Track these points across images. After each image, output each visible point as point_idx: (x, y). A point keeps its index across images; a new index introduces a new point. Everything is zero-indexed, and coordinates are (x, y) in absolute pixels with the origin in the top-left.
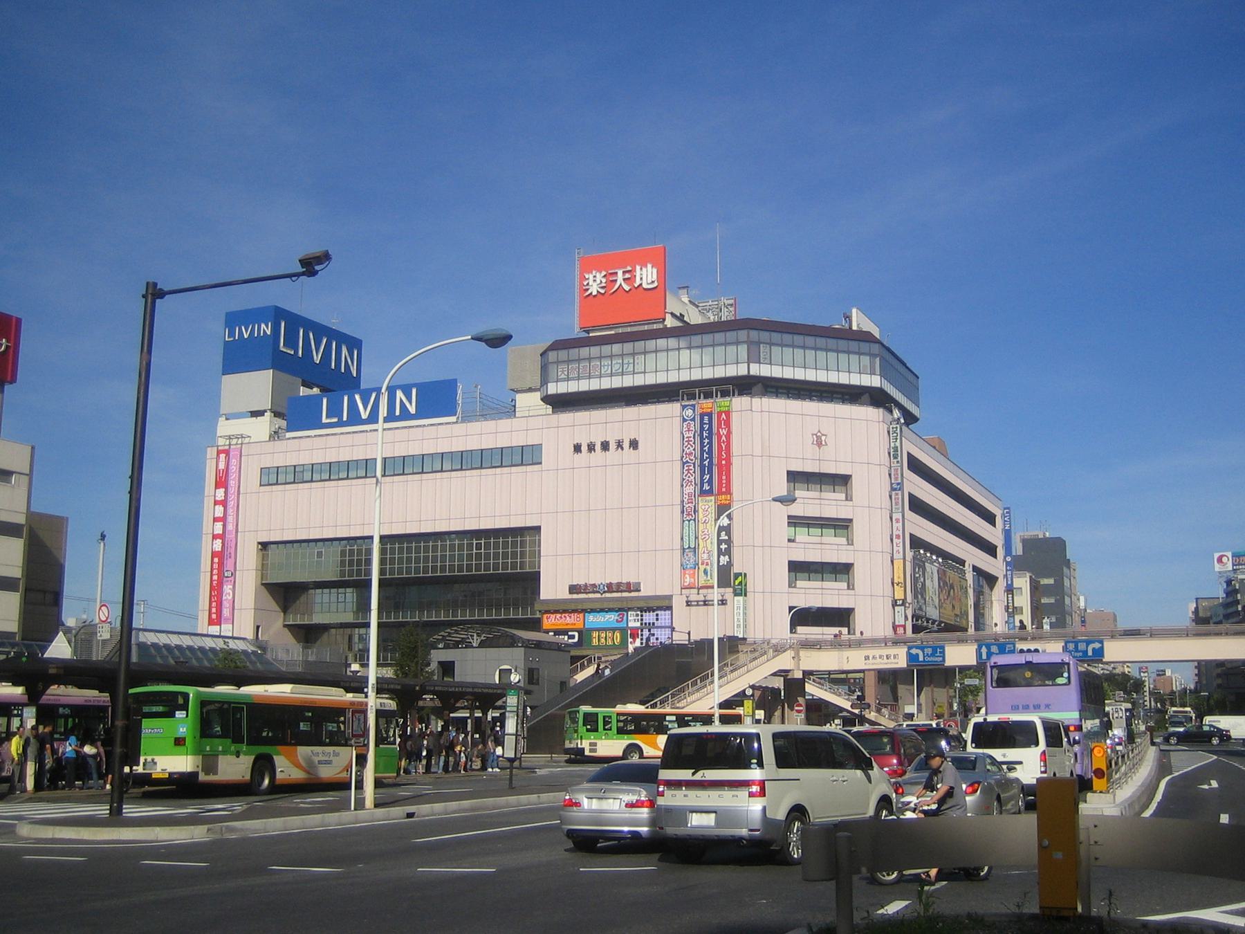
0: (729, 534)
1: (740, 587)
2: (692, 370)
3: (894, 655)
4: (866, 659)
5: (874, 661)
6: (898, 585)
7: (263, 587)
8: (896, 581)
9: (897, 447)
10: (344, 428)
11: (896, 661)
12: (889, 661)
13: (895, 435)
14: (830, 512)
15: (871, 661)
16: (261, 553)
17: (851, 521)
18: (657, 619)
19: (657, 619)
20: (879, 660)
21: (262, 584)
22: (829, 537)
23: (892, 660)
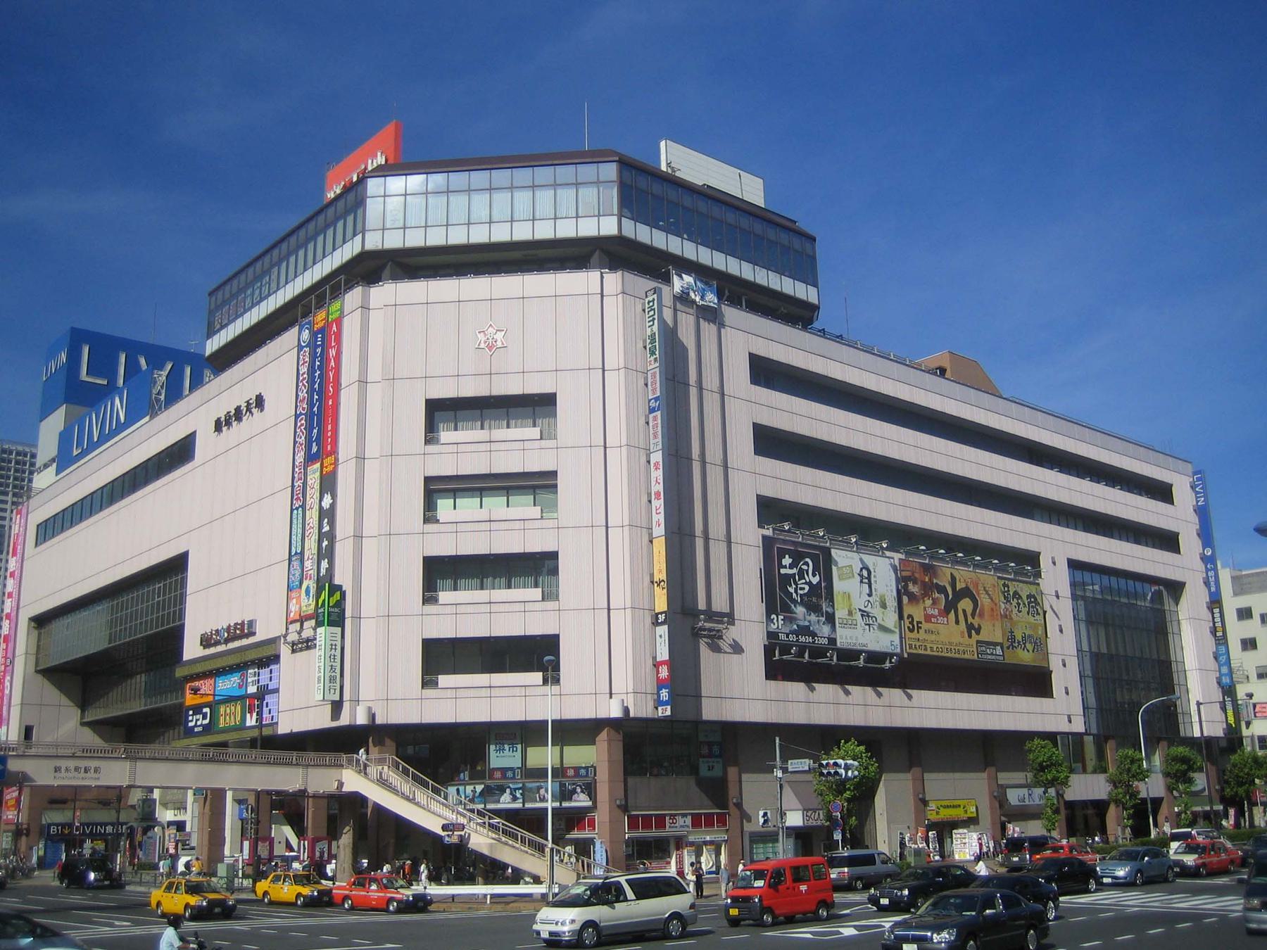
0: (332, 523)
1: (336, 610)
2: (385, 231)
3: (85, 768)
4: (56, 771)
5: (70, 775)
6: (658, 585)
7: (40, 677)
8: (656, 579)
9: (655, 333)
10: (121, 435)
11: (96, 776)
12: (88, 775)
13: (652, 313)
14: (508, 462)
15: (63, 774)
16: (36, 632)
17: (553, 474)
18: (271, 680)
19: (271, 680)
20: (82, 774)
21: (37, 672)
22: (523, 507)
23: (91, 774)
